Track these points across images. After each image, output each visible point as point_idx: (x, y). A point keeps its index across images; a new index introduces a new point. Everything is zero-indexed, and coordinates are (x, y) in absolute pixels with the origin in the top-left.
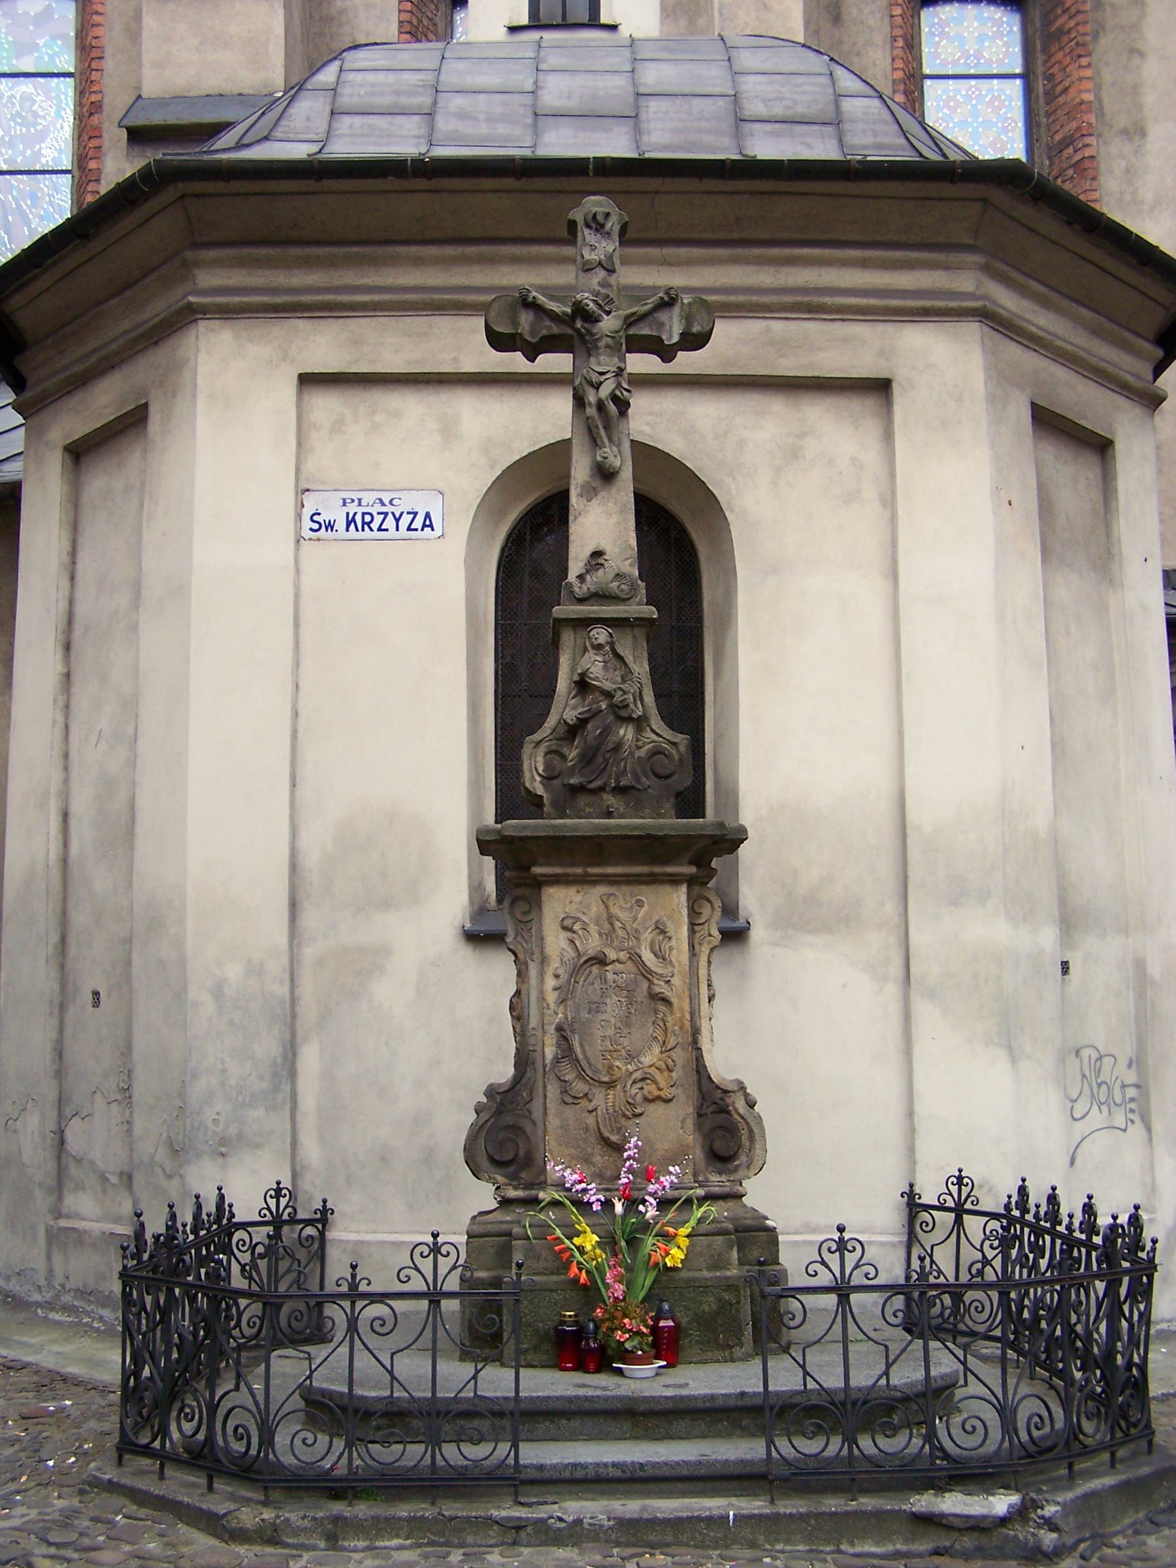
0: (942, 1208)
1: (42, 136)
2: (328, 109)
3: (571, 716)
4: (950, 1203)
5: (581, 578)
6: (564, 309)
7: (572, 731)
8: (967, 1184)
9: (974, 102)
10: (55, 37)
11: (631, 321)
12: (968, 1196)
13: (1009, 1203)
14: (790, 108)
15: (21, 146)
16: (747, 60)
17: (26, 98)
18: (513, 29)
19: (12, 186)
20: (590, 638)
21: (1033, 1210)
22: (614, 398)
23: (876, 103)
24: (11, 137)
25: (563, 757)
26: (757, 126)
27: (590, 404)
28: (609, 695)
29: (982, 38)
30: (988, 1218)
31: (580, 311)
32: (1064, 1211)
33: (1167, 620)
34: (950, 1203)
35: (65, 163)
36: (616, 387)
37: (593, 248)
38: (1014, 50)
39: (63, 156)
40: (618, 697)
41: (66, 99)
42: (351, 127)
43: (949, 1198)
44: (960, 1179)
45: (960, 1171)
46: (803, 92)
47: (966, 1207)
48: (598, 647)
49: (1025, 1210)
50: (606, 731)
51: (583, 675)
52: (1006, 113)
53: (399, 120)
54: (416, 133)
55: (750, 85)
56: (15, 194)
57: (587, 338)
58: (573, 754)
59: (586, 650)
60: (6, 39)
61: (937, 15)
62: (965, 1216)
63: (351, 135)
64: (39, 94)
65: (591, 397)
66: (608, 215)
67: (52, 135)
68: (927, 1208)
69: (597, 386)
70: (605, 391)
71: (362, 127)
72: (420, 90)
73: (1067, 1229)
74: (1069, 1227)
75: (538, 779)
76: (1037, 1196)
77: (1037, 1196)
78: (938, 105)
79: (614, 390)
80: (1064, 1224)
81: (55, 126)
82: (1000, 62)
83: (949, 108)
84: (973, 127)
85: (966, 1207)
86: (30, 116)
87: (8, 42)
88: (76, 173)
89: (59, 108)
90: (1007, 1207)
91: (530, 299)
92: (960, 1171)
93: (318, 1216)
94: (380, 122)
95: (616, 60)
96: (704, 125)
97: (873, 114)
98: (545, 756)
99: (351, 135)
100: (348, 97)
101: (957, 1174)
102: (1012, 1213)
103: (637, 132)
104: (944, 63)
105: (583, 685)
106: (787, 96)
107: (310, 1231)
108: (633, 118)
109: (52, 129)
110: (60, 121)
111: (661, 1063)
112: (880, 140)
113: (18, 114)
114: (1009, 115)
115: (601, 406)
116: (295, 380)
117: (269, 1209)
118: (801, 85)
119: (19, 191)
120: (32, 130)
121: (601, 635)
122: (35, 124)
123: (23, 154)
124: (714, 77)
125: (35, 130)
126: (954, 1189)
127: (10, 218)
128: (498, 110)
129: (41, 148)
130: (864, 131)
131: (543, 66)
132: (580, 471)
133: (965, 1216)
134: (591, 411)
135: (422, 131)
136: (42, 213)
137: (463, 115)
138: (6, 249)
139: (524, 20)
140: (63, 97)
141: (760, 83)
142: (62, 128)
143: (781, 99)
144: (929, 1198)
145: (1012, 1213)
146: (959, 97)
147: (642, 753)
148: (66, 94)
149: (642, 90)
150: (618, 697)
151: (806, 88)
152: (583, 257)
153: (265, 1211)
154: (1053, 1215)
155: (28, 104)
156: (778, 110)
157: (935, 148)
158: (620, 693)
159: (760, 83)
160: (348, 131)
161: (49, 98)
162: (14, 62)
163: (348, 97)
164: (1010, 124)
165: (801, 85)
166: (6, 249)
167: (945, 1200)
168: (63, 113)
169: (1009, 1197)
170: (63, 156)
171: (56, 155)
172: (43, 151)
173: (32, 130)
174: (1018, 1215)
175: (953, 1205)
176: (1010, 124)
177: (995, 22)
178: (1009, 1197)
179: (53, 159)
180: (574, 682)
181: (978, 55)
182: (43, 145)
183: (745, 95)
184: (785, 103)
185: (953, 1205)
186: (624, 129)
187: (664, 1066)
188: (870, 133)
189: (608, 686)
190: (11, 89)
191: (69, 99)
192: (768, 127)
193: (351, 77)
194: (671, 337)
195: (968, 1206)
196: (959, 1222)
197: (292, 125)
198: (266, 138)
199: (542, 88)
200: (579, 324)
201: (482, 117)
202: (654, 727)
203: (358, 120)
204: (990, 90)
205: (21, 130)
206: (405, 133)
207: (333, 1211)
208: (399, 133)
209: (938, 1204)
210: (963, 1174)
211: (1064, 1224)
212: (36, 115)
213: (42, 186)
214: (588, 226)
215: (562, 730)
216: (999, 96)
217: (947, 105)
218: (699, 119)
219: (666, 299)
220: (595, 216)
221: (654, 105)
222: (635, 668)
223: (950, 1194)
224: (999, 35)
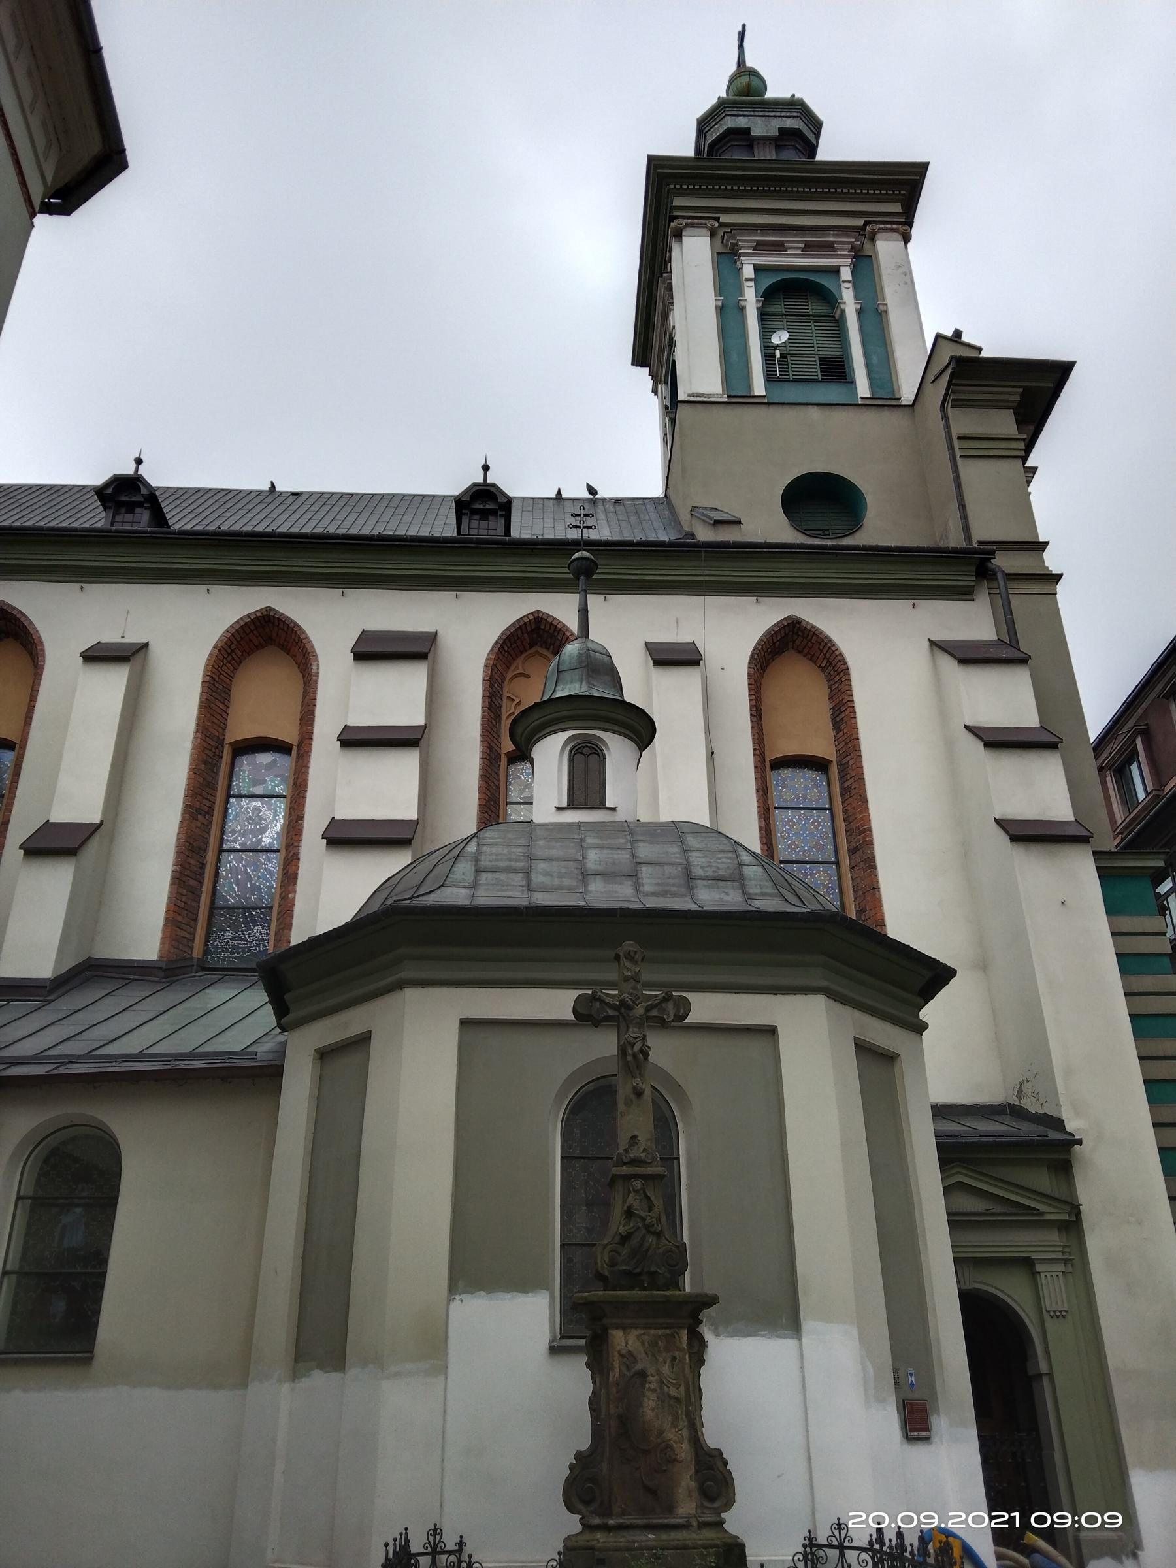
0: (831, 1546)
1: (264, 830)
2: (473, 869)
3: (623, 1230)
4: (835, 1543)
5: (626, 1150)
6: (615, 1002)
7: (625, 1239)
8: (844, 1529)
9: (803, 822)
10: (277, 776)
11: (648, 1009)
12: (846, 1537)
13: (871, 1540)
14: (716, 872)
15: (250, 836)
16: (692, 842)
17: (256, 809)
18: (559, 809)
19: (243, 859)
20: (632, 1185)
21: (887, 1544)
22: (641, 1051)
23: (760, 869)
24: (245, 830)
25: (619, 1254)
26: (699, 882)
27: (629, 1054)
28: (643, 1219)
29: (806, 788)
30: (860, 1552)
31: (623, 1003)
32: (907, 1543)
33: (939, 1145)
34: (835, 1543)
35: (276, 846)
36: (643, 1046)
37: (628, 969)
38: (824, 795)
39: (275, 842)
40: (648, 1221)
41: (280, 809)
42: (486, 879)
43: (834, 1539)
44: (839, 1525)
45: (839, 1519)
46: (723, 863)
47: (845, 1545)
48: (636, 1191)
49: (882, 1544)
50: (643, 1239)
51: (629, 1208)
52: (822, 829)
53: (511, 875)
54: (521, 884)
55: (696, 858)
56: (244, 863)
57: (627, 1018)
58: (624, 1251)
59: (629, 1192)
60: (248, 777)
61: (780, 775)
62: (845, 1551)
63: (487, 885)
64: (263, 807)
65: (629, 1051)
66: (636, 952)
67: (269, 830)
68: (821, 1546)
69: (633, 1045)
70: (637, 1048)
71: (492, 880)
72: (522, 858)
73: (910, 1555)
74: (912, 1553)
75: (606, 1267)
76: (890, 1535)
77: (890, 1535)
78: (783, 823)
79: (641, 1047)
80: (908, 1552)
81: (272, 825)
82: (817, 801)
83: (789, 826)
84: (803, 837)
85: (845, 1545)
86: (257, 819)
87: (249, 779)
88: (283, 852)
89: (276, 815)
90: (871, 1543)
91: (597, 997)
92: (839, 1519)
93: (457, 1548)
94: (503, 876)
95: (622, 841)
96: (672, 881)
97: (759, 876)
98: (609, 1252)
99: (487, 885)
100: (485, 862)
101: (837, 1522)
102: (874, 1547)
103: (637, 885)
104: (785, 801)
105: (629, 1213)
106: (714, 865)
107: (453, 1558)
108: (633, 876)
109: (270, 826)
110: (275, 822)
111: (676, 1438)
112: (764, 890)
113: (250, 818)
114: (824, 830)
115: (635, 1056)
116: (458, 1023)
117: (429, 1543)
118: (720, 859)
119: (246, 860)
120: (258, 827)
121: (637, 1183)
122: (260, 823)
123: (251, 840)
124: (674, 851)
125: (260, 827)
126: (836, 1533)
127: (240, 877)
128: (563, 870)
129: (262, 837)
130: (756, 885)
131: (585, 845)
132: (623, 1091)
133: (845, 1551)
134: (630, 1058)
135: (524, 883)
136: (259, 874)
137: (547, 874)
138: (236, 895)
139: (565, 805)
140: (278, 809)
141: (699, 857)
142: (276, 826)
143: (710, 866)
144: (822, 1540)
145: (874, 1547)
146: (794, 820)
147: (661, 1251)
148: (280, 807)
149: (638, 860)
150: (648, 1221)
151: (724, 860)
152: (623, 974)
153: (427, 1545)
154: (901, 1546)
155: (257, 812)
156: (710, 873)
157: (793, 892)
158: (649, 1218)
159: (699, 857)
160: (485, 882)
161: (269, 809)
162: (251, 789)
163: (485, 862)
164: (824, 835)
165: (720, 859)
166: (236, 895)
167: (832, 1541)
168: (277, 818)
169: (871, 1535)
170: (275, 842)
171: (271, 841)
172: (263, 839)
173: (258, 827)
174: (879, 1548)
175: (837, 1544)
176: (824, 835)
177: (814, 780)
178: (871, 1535)
179: (269, 843)
180: (625, 1211)
181: (804, 797)
182: (263, 835)
183: (691, 864)
184: (714, 869)
185: (837, 1544)
186: (630, 883)
187: (678, 1440)
188: (758, 887)
189: (643, 1214)
190: (247, 804)
191: (282, 810)
192: (705, 882)
193: (484, 849)
194: (668, 1017)
195: (846, 1544)
196: (842, 1555)
197: (455, 877)
198: (442, 886)
199: (586, 858)
200: (623, 1010)
201: (555, 874)
202: (667, 1237)
203: (490, 875)
204: (812, 816)
205: (251, 827)
206: (516, 884)
207: (466, 1544)
208: (512, 883)
209: (827, 1544)
210: (841, 1522)
211: (908, 1552)
212: (261, 818)
213: (261, 859)
214: (626, 958)
215: (617, 1239)
216: (817, 819)
217: (788, 824)
218: (669, 878)
219: (666, 997)
220: (629, 952)
221: (644, 869)
222: (656, 1203)
223: (835, 1537)
224: (815, 786)
